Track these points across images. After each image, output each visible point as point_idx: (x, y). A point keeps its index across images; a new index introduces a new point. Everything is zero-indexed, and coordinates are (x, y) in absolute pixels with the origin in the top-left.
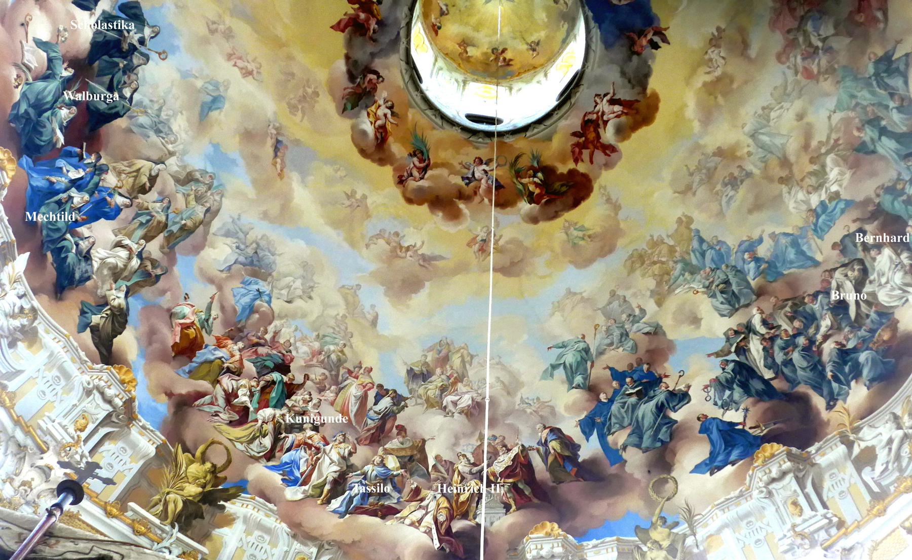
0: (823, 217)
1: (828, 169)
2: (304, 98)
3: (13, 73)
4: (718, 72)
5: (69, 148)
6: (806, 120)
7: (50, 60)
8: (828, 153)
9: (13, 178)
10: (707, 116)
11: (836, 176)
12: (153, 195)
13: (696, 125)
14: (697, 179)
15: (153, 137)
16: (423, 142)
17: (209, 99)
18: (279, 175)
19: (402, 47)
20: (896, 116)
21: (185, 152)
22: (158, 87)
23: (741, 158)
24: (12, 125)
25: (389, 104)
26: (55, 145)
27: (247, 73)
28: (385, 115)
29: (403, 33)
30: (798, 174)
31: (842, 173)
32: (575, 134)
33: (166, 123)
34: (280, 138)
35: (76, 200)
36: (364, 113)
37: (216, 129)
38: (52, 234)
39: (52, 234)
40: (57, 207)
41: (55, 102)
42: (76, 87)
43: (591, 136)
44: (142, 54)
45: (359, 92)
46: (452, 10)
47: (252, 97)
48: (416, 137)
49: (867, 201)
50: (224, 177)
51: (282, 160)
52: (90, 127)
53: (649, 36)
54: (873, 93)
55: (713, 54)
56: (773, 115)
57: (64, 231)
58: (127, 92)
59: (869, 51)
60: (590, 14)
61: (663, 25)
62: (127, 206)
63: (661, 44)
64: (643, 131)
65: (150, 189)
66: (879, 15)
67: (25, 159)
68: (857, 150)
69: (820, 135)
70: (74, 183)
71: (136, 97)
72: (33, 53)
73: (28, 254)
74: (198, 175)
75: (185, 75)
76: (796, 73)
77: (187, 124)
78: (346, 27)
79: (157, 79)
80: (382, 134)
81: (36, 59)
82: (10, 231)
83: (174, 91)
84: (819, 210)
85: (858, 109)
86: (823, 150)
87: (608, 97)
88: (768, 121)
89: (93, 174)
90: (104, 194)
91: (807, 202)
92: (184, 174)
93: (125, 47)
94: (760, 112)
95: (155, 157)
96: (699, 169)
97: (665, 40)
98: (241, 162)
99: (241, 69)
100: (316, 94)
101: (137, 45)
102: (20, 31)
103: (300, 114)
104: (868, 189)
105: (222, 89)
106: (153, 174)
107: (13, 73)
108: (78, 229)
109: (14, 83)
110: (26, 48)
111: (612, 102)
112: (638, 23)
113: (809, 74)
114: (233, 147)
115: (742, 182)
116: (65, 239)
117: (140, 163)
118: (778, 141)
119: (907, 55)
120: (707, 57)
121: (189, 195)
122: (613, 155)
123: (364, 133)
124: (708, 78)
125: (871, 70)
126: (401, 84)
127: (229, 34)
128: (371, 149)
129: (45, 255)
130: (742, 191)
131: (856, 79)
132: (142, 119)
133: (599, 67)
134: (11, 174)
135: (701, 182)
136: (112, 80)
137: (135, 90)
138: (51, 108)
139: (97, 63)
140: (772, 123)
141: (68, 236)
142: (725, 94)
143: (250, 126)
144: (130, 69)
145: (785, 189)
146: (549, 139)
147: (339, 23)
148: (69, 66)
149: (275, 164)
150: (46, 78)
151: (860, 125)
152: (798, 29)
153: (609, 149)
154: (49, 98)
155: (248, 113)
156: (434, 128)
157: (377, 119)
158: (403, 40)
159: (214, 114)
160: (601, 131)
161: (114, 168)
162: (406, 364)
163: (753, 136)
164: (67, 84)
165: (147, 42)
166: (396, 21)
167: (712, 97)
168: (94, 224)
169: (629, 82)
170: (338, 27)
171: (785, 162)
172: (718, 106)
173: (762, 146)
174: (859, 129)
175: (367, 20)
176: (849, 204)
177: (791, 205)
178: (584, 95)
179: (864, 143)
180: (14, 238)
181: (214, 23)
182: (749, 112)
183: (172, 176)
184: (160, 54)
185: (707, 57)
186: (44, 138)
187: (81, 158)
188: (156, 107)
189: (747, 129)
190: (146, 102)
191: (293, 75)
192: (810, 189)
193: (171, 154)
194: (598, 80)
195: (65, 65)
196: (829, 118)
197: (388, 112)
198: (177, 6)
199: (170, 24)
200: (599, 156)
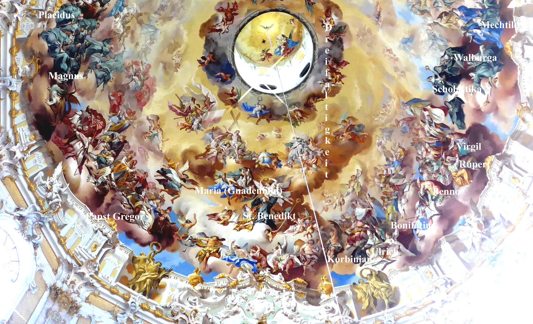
0: (120, 6)
1: (122, 26)
2: (364, 35)
3: (497, 84)
4: (175, 53)
5: (478, 43)
6: (135, 44)
7: (479, 83)
8: (123, 33)
9: (507, 41)
10: (177, 33)
11: (117, 24)
12: (442, 10)
13: (182, 28)
14: (179, 5)
15: (437, 35)
16: (308, 8)
17: (409, 43)
18: (379, 4)
19: (317, 51)
20: (97, 60)
21: (423, 24)
22: (432, 55)
23: (160, 19)
24: (502, 63)
25: (324, 26)
26: (484, 47)
27: (389, 51)
28: (326, 22)
29: (317, 57)
30: (135, 20)
31: (115, 27)
32: (237, 14)
33: (430, 39)
34: (377, 19)
36: (336, 24)
37: (407, 30)
41: (480, 65)
42: (469, 67)
43: (229, 15)
44: (437, 71)
45: (338, 34)
46: (289, 22)
47: (389, 40)
48: (312, 11)
49: (102, 20)
50: (406, 9)
51: (377, 9)
52: (467, 47)
53: (206, 61)
54: (108, 65)
55: (178, 60)
56: (149, 41)
58: (446, 57)
59: (114, 82)
60: (233, 67)
61: (201, 67)
62: (455, 9)
63: (201, 59)
64: (205, 20)
65: (443, 13)
66: (112, 98)
67: (500, 47)
68: (110, 39)
69: (127, 40)
70: (479, 28)
71: (443, 54)
72: (486, 89)
73: (508, 7)
74: (418, 13)
75: (418, 57)
76: (142, 62)
77: (420, 35)
78: (343, 63)
79: (433, 59)
80: (328, 13)
81: (485, 85)
82: (514, 60)
83: (425, 51)
84: (122, 7)
85: (113, 56)
86: (125, 34)
87: (222, 32)
88: (150, 38)
89: (469, 28)
90: (465, 18)
91: (128, 9)
92: (425, 15)
93: (444, 77)
94: (155, 41)
95: (437, 26)
96: (179, 10)
97: (199, 61)
98: (397, 13)
99: (392, 53)
100: (358, 36)
101: (438, 75)
102: (490, 99)
103: (366, 28)
104: (103, 25)
105: (402, 46)
106: (440, 19)
107: (497, 84)
108: (481, 8)
109: (498, 80)
110: (489, 92)
111: (220, 30)
112: (212, 67)
113: (136, 63)
114: (400, 20)
115: (159, 9)
117: (446, 25)
118: (145, 30)
119: (98, 86)
120: (180, 58)
121: (424, 5)
122: (219, 8)
123: (336, 15)
124: (179, 49)
125: (111, 75)
126: (318, 35)
127: (396, 69)
128: (333, 8)
129: (500, 3)
130: (158, 5)
131: (117, 69)
132: (441, 43)
133: (227, 45)
134: (507, 43)
135: (177, 4)
136: (453, 64)
137: (442, 57)
138: (483, 63)
139: (458, 74)
140: (149, 38)
141: (487, 7)
142: (171, 44)
143: (390, 27)
144: (444, 67)
145: (139, 11)
146: (248, 11)
147: (345, 65)
148: (471, 77)
149: (380, 9)
150: (483, 76)
151: (112, 50)
152: (144, 80)
153: (221, 10)
154: (483, 67)
155: (391, 34)
156: (303, 14)
157: (330, 21)
158: (316, 54)
159: (407, 36)
160: (225, 17)
161: (458, 27)
163: (156, 29)
164: (473, 70)
165: (434, 76)
166: (319, 62)
167: (176, 41)
168: (473, 7)
169: (213, 40)
170: (346, 63)
171: (140, 23)
172: (173, 39)
173: (151, 26)
174: (112, 48)
175: (333, 65)
176: (110, 15)
177: (135, 6)
178: (233, 32)
179: (108, 43)
180: (514, 16)
181: (402, 76)
182: (160, 38)
183: (431, 15)
184: (429, 69)
185: (180, 58)
186: (489, 52)
187: (473, 37)
188: (434, 47)
189: (159, 32)
190: (438, 50)
191: (368, 46)
192: (128, 15)
193: (430, 25)
194: (227, 39)
195: (473, 78)
196: (125, 48)
197: (324, 23)
198: (418, 87)
199: (423, 81)
200: (225, 7)
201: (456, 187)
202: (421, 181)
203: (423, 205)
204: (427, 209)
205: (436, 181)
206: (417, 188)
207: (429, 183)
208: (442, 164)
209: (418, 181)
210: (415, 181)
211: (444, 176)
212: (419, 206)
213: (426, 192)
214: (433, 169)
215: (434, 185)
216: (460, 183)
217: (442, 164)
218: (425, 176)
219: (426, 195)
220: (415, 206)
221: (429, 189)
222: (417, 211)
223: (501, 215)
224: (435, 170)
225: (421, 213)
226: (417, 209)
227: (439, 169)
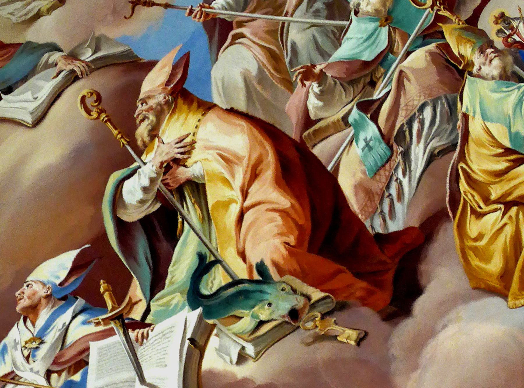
201: (442, 277)
202: (183, 94)
203: (95, 303)
204: (107, 354)
205: (302, 150)
206: (116, 142)
207: (239, 140)
208: (431, 33)
209: (154, 84)
210: (136, 66)
211: (396, 140)
212: (60, 296)
213: (177, 197)
214: (338, 36)
215: (269, 173)
216: (495, 265)
217: (431, 33)
218: (235, 67)
219: (162, 227)
220: (20, 279)
221: (214, 194)
222: (19, 333)
223: (186, 319)
224: (346, 50)
225: (40, 365)
226: (33, 310)
227: (383, 59)
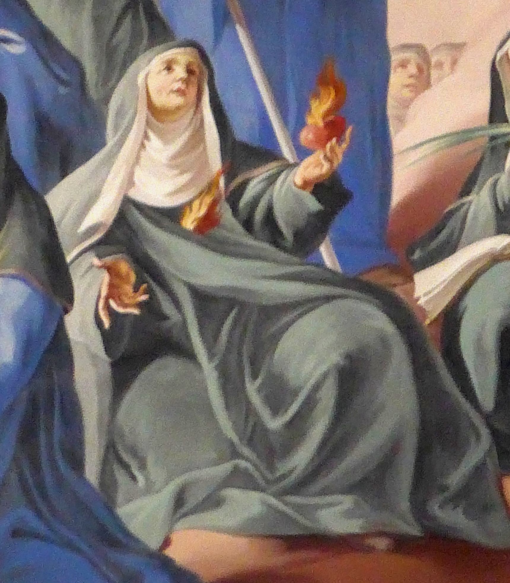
35: (158, 189)
38: (366, 448)
39: (366, 448)
40: (164, 370)
57: (380, 322)
116: (451, 318)
141: (431, 286)
162: (160, 72)
